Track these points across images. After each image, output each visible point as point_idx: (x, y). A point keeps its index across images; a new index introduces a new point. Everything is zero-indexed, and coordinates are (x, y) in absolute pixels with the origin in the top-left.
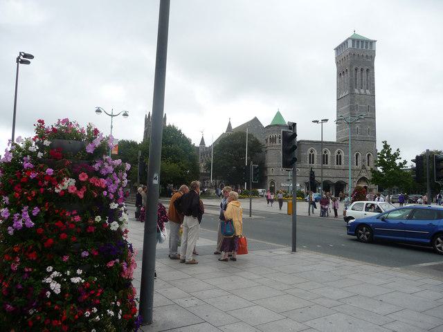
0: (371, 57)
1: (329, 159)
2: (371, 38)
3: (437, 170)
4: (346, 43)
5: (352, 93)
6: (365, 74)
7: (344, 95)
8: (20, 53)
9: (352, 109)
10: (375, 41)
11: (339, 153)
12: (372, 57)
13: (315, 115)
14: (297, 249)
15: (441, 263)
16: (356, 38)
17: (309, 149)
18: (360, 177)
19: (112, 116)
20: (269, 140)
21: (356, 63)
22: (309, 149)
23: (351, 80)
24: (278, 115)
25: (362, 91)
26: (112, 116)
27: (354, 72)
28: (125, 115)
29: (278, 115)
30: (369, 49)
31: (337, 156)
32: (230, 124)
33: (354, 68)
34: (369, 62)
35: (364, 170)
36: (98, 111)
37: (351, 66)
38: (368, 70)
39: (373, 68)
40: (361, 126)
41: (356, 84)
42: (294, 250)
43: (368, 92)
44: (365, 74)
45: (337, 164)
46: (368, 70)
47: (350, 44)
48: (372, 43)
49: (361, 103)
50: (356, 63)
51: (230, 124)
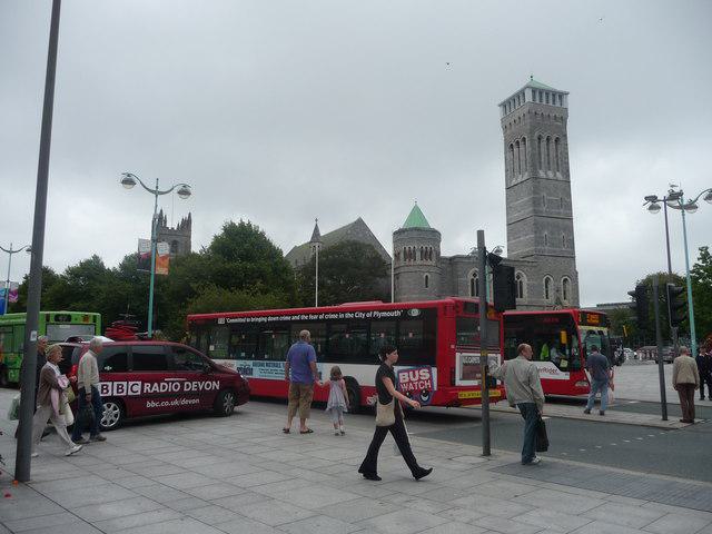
2: (559, 88)
3: (674, 309)
4: (520, 95)
5: (535, 178)
6: (552, 145)
7: (519, 180)
9: (536, 202)
12: (563, 120)
13: (474, 216)
14: (492, 451)
15: (709, 484)
16: (536, 86)
19: (11, 252)
20: (402, 255)
23: (533, 155)
24: (416, 212)
25: (551, 175)
26: (11, 252)
29: (416, 212)
30: (558, 104)
32: (316, 229)
33: (536, 134)
34: (557, 126)
37: (531, 132)
38: (557, 140)
39: (566, 136)
40: (552, 233)
41: (540, 162)
42: (487, 453)
43: (559, 175)
44: (552, 145)
46: (557, 140)
47: (529, 96)
48: (562, 95)
51: (316, 229)
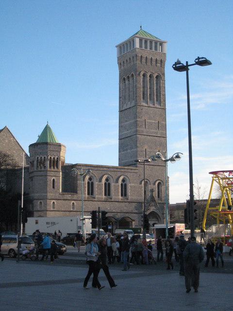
2: (163, 39)
35: (153, 204)
38: (157, 77)
49: (150, 119)
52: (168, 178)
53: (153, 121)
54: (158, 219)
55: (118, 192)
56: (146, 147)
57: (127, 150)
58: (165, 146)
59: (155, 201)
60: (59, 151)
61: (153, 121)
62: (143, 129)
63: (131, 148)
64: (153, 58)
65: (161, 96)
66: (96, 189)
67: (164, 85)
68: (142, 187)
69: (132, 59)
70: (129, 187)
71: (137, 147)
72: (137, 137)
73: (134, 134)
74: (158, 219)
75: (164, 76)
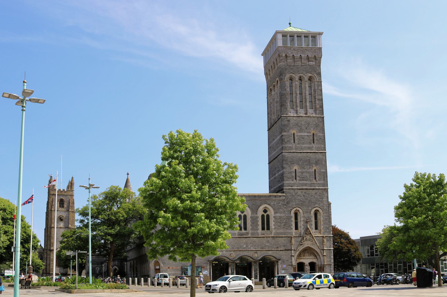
0: (316, 57)
1: (260, 223)
2: (314, 29)
8: (235, 167)
10: (321, 34)
11: (265, 211)
17: (261, 208)
18: (301, 248)
21: (293, 73)
22: (261, 208)
27: (288, 83)
28: (128, 174)
31: (263, 216)
35: (308, 237)
36: (128, 174)
38: (310, 79)
39: (319, 74)
45: (263, 229)
49: (301, 131)
50: (293, 73)
52: (329, 204)
53: (306, 134)
54: (316, 256)
55: (257, 225)
56: (296, 167)
57: (275, 174)
58: (324, 163)
59: (311, 234)
60: (396, 214)
61: (306, 134)
62: (290, 145)
63: (279, 171)
64: (303, 56)
65: (317, 102)
66: (273, 223)
67: (320, 88)
68: (291, 217)
69: (275, 62)
70: (273, 219)
71: (283, 168)
72: (283, 156)
73: (281, 152)
74: (316, 256)
75: (320, 77)
